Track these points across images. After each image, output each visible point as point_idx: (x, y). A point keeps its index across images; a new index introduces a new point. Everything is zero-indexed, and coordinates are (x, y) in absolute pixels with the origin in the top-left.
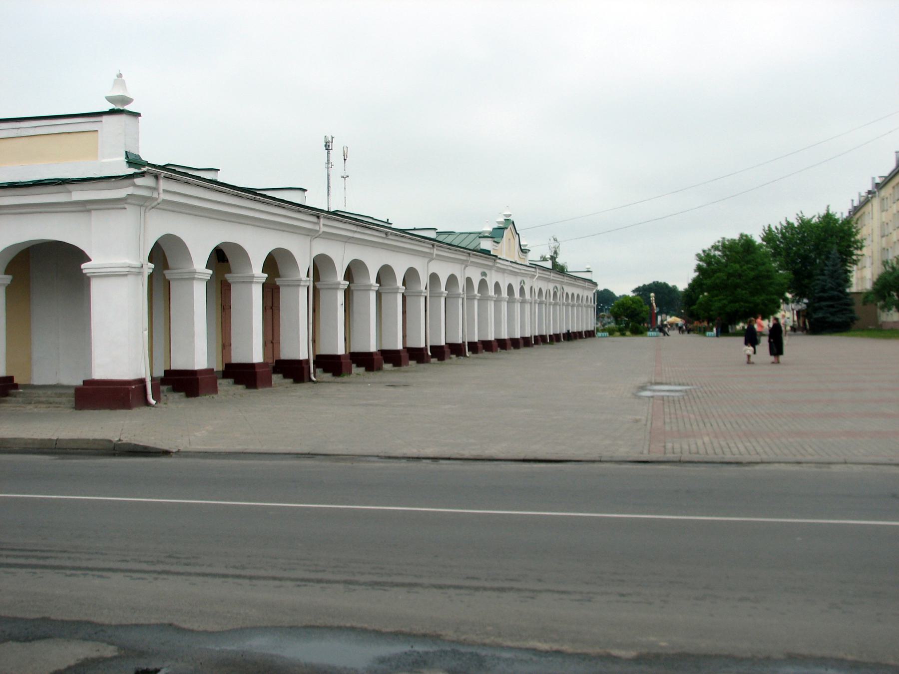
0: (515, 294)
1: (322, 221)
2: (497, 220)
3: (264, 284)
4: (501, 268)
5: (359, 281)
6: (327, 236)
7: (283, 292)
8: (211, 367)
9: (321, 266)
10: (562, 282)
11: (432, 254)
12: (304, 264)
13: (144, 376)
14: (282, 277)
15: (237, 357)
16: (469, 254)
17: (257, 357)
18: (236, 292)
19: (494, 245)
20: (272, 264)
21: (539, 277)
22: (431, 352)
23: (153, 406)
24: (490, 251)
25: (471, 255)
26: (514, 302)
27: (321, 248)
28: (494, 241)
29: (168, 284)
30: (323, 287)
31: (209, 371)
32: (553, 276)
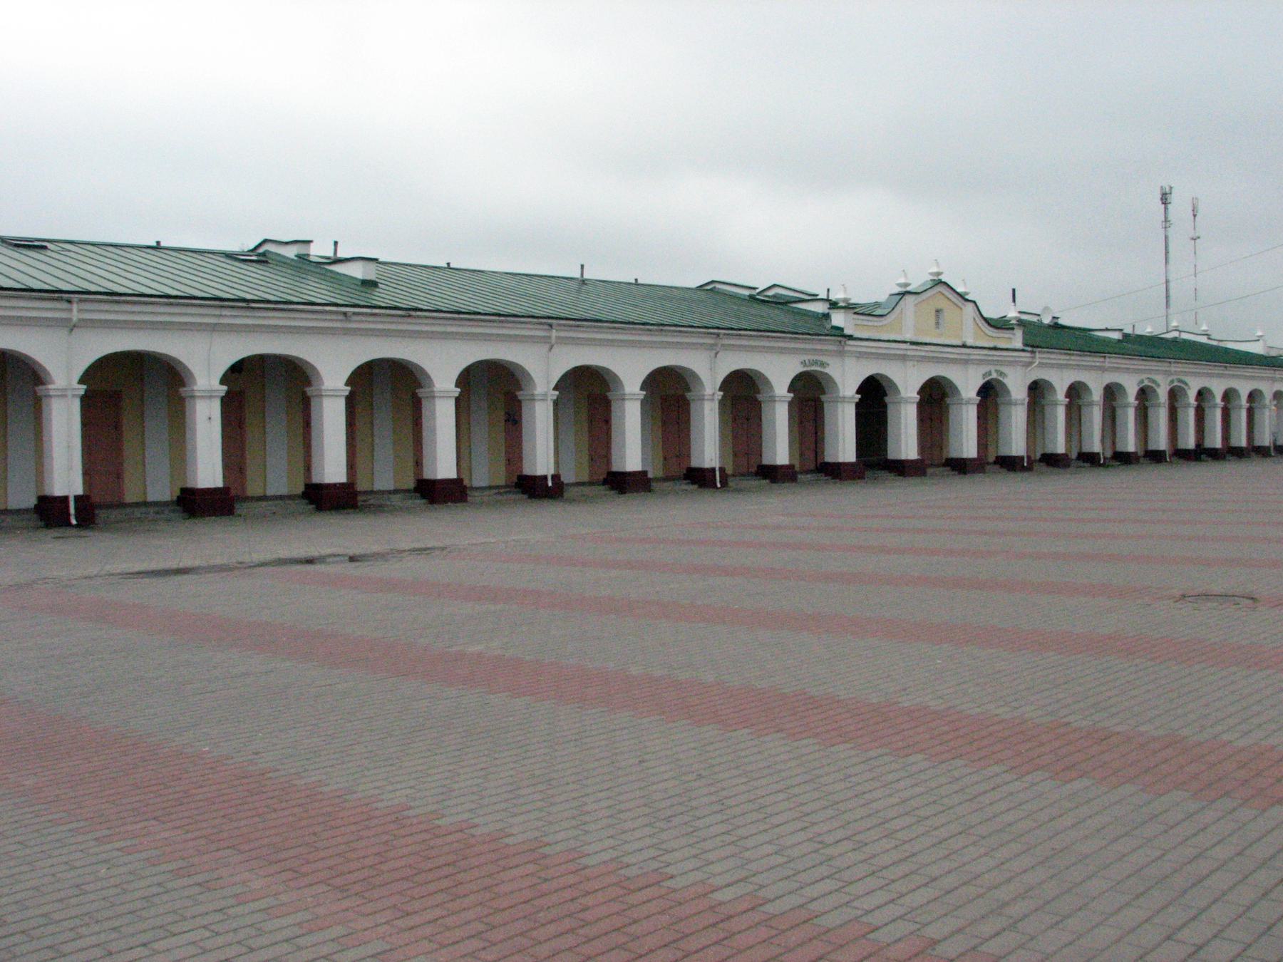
1: (75, 307)
2: (898, 282)
3: (223, 399)
4: (30, 318)
5: (1233, 403)
7: (1207, 411)
8: (645, 469)
9: (1112, 392)
11: (550, 337)
14: (49, 384)
15: (1152, 447)
16: (551, 325)
18: (1151, 412)
21: (1040, 363)
22: (77, 518)
23: (717, 488)
24: (842, 329)
25: (721, 336)
27: (732, 362)
28: (855, 313)
29: (1079, 408)
31: (1135, 453)
32: (1109, 363)
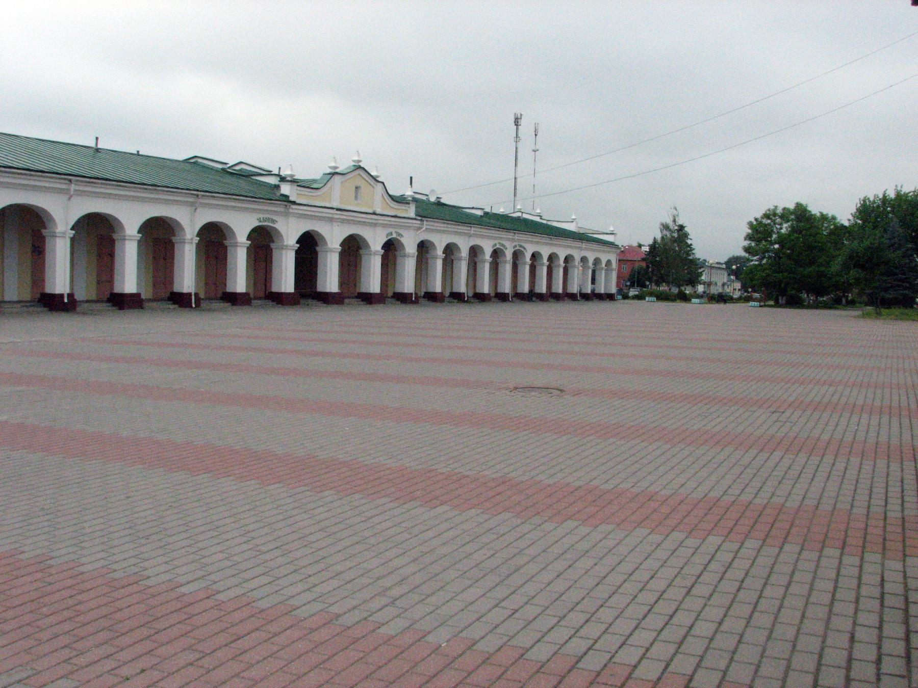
0: (328, 243)
3: (382, 256)
5: (556, 263)
6: (586, 249)
9: (475, 251)
10: (513, 239)
11: (69, 190)
12: (464, 253)
13: (190, 292)
16: (70, 181)
17: (560, 291)
19: (297, 190)
20: (534, 256)
21: (426, 229)
26: (371, 254)
27: (584, 253)
30: (119, 238)
31: (488, 294)
